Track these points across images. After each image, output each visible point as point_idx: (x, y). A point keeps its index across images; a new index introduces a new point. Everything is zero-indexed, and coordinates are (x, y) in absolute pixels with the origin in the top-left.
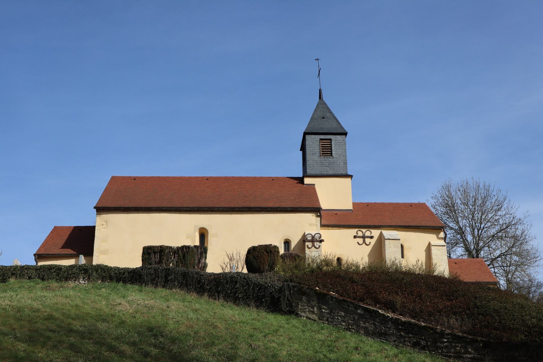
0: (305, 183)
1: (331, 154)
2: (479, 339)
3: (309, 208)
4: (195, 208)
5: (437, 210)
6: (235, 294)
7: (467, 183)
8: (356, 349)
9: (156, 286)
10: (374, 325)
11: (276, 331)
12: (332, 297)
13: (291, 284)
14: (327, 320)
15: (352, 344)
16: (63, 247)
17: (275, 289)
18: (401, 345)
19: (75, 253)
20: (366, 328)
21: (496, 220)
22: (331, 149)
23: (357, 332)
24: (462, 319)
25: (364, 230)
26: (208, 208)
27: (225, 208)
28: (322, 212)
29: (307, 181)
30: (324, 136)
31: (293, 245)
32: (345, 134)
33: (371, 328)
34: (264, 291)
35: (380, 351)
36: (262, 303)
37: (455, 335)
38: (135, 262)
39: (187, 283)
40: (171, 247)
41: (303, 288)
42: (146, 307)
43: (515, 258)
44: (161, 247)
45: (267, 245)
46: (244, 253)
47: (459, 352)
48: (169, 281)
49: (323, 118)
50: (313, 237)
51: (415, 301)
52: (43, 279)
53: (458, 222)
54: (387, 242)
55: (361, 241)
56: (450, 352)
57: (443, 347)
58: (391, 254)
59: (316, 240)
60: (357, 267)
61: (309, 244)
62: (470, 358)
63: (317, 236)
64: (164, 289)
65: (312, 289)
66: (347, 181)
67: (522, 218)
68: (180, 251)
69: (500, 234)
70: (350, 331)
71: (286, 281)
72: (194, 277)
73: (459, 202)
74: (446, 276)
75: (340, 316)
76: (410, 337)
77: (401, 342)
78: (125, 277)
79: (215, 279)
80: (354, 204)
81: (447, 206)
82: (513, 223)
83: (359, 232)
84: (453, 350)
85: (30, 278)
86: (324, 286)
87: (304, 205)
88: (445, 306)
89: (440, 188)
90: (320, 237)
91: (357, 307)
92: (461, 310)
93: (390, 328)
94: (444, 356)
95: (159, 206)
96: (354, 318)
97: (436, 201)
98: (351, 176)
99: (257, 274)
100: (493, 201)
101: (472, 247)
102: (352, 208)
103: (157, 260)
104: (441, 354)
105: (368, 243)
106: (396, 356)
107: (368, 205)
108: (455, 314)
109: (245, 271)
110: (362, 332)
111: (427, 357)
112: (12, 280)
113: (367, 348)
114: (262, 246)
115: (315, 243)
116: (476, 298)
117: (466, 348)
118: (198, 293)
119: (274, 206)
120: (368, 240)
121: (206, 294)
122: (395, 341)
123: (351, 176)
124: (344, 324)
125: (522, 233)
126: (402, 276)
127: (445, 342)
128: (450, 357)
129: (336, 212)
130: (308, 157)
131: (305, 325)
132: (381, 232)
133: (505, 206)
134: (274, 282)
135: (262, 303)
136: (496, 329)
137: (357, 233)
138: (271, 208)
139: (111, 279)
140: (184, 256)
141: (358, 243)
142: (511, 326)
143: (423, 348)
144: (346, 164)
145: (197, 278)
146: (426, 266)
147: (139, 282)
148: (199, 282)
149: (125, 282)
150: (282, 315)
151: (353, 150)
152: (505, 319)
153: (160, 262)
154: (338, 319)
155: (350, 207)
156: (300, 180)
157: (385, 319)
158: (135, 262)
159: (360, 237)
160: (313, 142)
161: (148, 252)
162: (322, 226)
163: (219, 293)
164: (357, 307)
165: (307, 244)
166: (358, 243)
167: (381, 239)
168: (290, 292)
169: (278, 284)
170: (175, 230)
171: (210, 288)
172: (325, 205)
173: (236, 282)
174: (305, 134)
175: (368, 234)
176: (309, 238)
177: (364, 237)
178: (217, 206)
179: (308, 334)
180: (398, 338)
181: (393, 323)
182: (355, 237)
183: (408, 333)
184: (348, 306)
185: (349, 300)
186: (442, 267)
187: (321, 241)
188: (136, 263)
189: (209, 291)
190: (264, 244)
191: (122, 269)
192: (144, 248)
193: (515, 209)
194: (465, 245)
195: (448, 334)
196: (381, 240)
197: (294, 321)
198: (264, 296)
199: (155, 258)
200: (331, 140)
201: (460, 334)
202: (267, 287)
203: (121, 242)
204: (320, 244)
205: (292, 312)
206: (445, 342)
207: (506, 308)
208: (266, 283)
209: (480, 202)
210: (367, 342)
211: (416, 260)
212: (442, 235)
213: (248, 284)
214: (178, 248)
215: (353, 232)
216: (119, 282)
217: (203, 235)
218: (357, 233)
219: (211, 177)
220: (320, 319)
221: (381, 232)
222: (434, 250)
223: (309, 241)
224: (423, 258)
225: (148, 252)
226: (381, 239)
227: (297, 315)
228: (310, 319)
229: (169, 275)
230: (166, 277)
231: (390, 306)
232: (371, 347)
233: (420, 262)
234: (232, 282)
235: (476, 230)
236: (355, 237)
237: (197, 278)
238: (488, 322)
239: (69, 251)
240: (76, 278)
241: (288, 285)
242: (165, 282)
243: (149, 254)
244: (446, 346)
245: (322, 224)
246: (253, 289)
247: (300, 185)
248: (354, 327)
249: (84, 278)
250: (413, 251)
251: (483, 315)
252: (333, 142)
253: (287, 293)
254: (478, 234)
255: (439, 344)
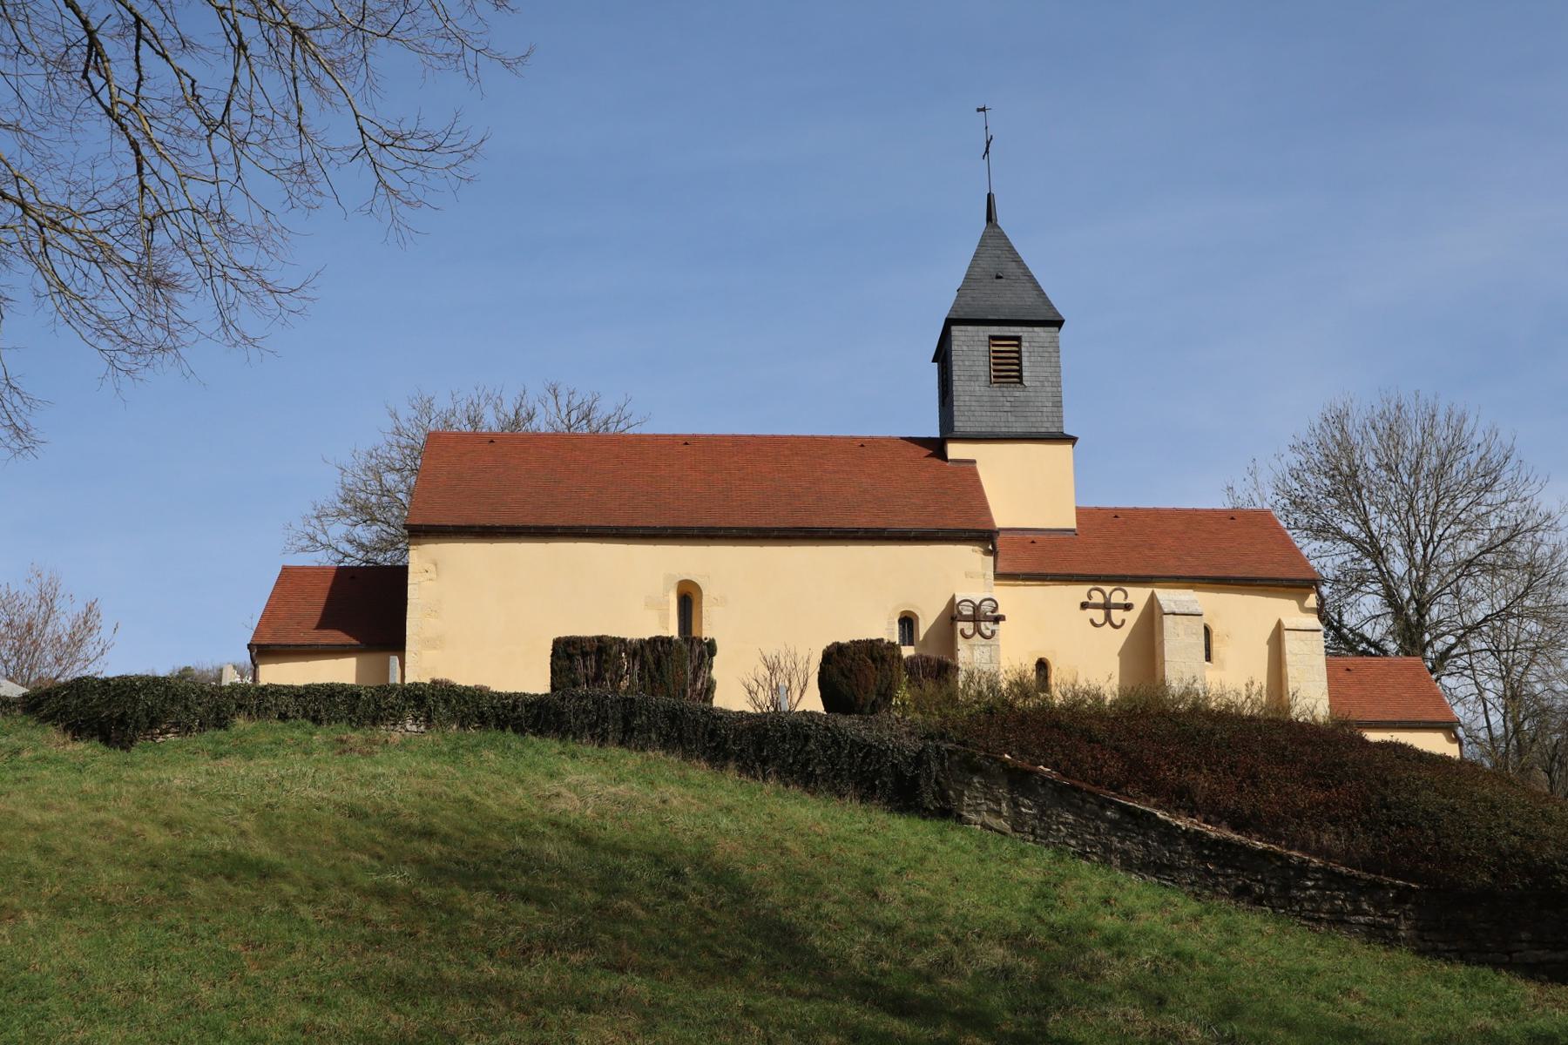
0: (950, 457)
1: (1020, 377)
2: (1387, 880)
3: (965, 531)
4: (665, 528)
5: (1306, 484)
6: (805, 765)
7: (1399, 408)
8: (1106, 902)
9: (603, 740)
10: (1146, 845)
11: (922, 860)
12: (1044, 781)
13: (944, 746)
14: (1033, 833)
15: (1095, 892)
16: (322, 625)
17: (905, 758)
18: (1207, 892)
19: (354, 642)
20: (1126, 852)
21: (1478, 517)
22: (1020, 364)
23: (1105, 861)
24: (1351, 833)
25: (1107, 589)
26: (700, 528)
27: (746, 529)
28: (999, 541)
29: (955, 451)
30: (999, 326)
31: (923, 628)
32: (1058, 323)
33: (1138, 853)
34: (878, 762)
35: (1162, 908)
36: (873, 788)
37: (1332, 872)
38: (531, 677)
39: (680, 735)
40: (623, 640)
41: (973, 755)
42: (617, 802)
43: (1532, 626)
44: (600, 639)
45: (871, 641)
46: (817, 658)
47: (1341, 911)
48: (633, 730)
49: (998, 277)
50: (976, 608)
51: (1240, 789)
52: (316, 720)
53: (1365, 522)
54: (1168, 621)
55: (1099, 615)
56: (1319, 911)
57: (1304, 899)
58: (1181, 668)
59: (985, 617)
60: (1098, 699)
61: (968, 627)
62: (1366, 924)
63: (986, 608)
64: (625, 751)
65: (996, 760)
66: (1061, 453)
67: (1555, 511)
68: (648, 651)
69: (1489, 557)
70: (1088, 859)
71: (930, 736)
72: (698, 722)
73: (1371, 461)
74: (1321, 720)
75: (1064, 824)
76: (1228, 876)
77: (1206, 887)
78: (519, 717)
79: (752, 729)
80: (1081, 513)
81: (1333, 472)
82: (1529, 524)
83: (1094, 593)
84: (1327, 906)
85: (283, 717)
86: (1023, 750)
87: (952, 523)
88: (1310, 803)
89: (1317, 421)
90: (996, 609)
91: (1105, 804)
92: (1348, 812)
93: (1181, 855)
94: (1305, 918)
95: (571, 523)
96: (1097, 829)
97: (1303, 460)
98: (1072, 440)
99: (855, 718)
100: (1474, 459)
101: (1407, 594)
102: (1073, 525)
103: (591, 673)
104: (1299, 914)
105: (1118, 623)
106: (1196, 919)
107: (1116, 514)
108: (1334, 821)
109: (819, 707)
110: (1117, 862)
111: (1265, 921)
112: (241, 723)
113: (1130, 901)
114: (859, 642)
115: (983, 625)
116: (1386, 783)
117: (1355, 902)
118: (711, 761)
119: (873, 525)
120: (1117, 615)
121: (732, 765)
122: (1193, 884)
123: (1072, 440)
124: (1073, 842)
125: (1552, 558)
126: (1209, 725)
127: (1309, 888)
128: (1319, 921)
129: (1032, 536)
130: (958, 386)
131: (982, 846)
132: (1153, 594)
133: (1506, 476)
134: (888, 727)
135: (873, 788)
136: (1427, 858)
137: (1090, 597)
138: (867, 530)
139: (483, 721)
140: (658, 662)
141: (1092, 621)
142: (1462, 853)
143: (1258, 901)
144: (1058, 404)
145: (706, 725)
146: (1269, 695)
147: (557, 730)
148: (713, 734)
149: (520, 730)
150: (924, 818)
151: (1076, 363)
152: (1448, 836)
153: (598, 678)
154: (1059, 830)
155: (1070, 522)
156: (936, 448)
157: (1169, 834)
158: (531, 677)
159: (1096, 606)
160: (971, 346)
161: (566, 652)
162: (1000, 576)
163: (764, 762)
164: (1105, 804)
165: (960, 625)
166: (1092, 621)
167: (1153, 612)
168: (942, 764)
169: (912, 745)
170: (621, 591)
171: (742, 750)
172: (1004, 515)
173: (807, 738)
174: (950, 323)
175: (1118, 597)
176: (967, 611)
177: (1107, 607)
178: (723, 525)
179: (993, 866)
180: (1200, 877)
181: (1189, 842)
182: (1084, 606)
183: (1223, 867)
184: (1083, 800)
185: (1085, 786)
186: (1311, 693)
187: (998, 620)
188: (536, 680)
189: (739, 757)
190: (863, 638)
191: (509, 696)
192: (557, 642)
193: (1537, 485)
194: (1387, 588)
195: (1317, 870)
196: (1152, 616)
197: (957, 837)
198: (878, 774)
199: (585, 666)
200: (1018, 338)
201: (1343, 869)
202: (885, 752)
203: (487, 618)
204: (995, 627)
205: (947, 813)
206: (1309, 888)
207: (1454, 810)
208: (882, 741)
209: (1435, 461)
210: (1128, 885)
211: (1246, 680)
212: (1312, 601)
213: (835, 741)
214: (643, 644)
215: (1080, 592)
216: (503, 729)
217: (688, 599)
218: (1090, 597)
219: (695, 436)
220: (1015, 830)
221: (1153, 594)
222: (1291, 643)
223: (966, 619)
224: (1261, 678)
225: (566, 652)
226: (1153, 612)
227: (959, 818)
228: (991, 829)
229: (634, 714)
230: (626, 720)
231: (1181, 799)
232: (1138, 897)
233: (1255, 689)
234: (796, 736)
235: (1419, 544)
236: (1084, 606)
237: (706, 725)
238: (1410, 842)
239: (337, 637)
240: (397, 718)
241: (938, 747)
242: (625, 733)
243: (570, 657)
244: (1312, 899)
245: (999, 571)
246: (851, 755)
247: (938, 462)
248: (1099, 849)
249: (416, 719)
250: (1240, 651)
251: (1400, 825)
252: (1025, 344)
253: (935, 766)
254: (1424, 556)
255: (1294, 892)
